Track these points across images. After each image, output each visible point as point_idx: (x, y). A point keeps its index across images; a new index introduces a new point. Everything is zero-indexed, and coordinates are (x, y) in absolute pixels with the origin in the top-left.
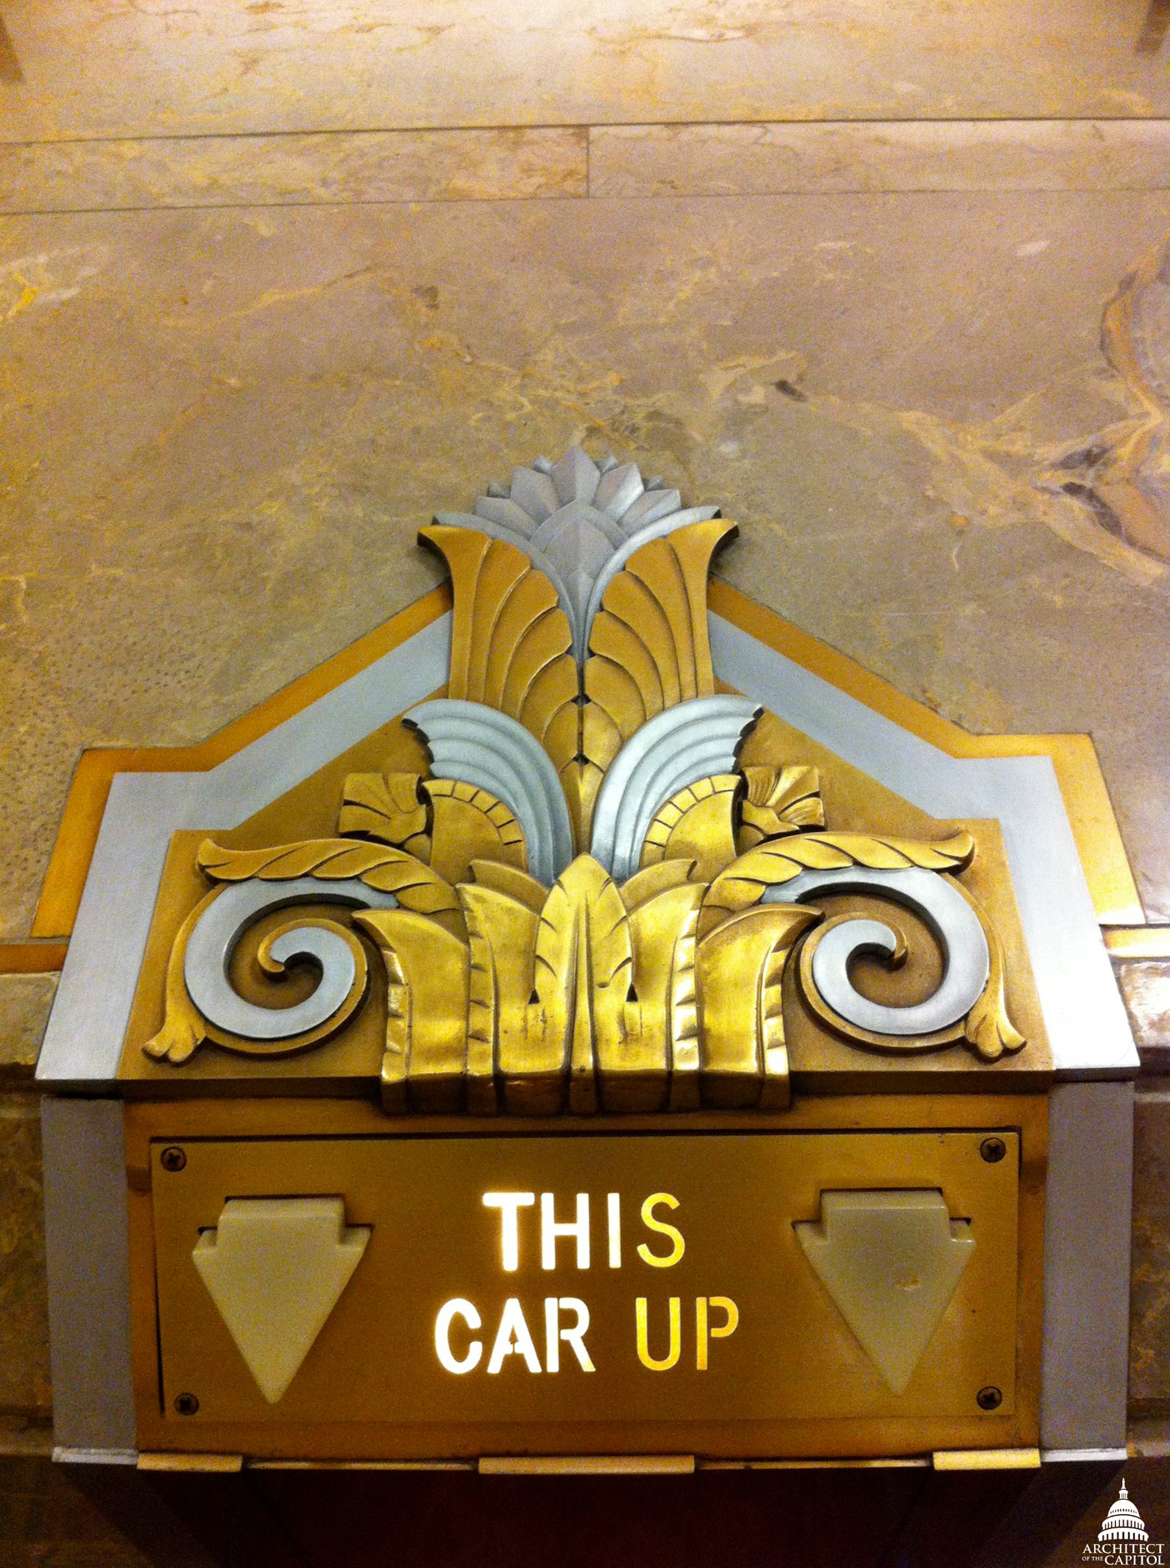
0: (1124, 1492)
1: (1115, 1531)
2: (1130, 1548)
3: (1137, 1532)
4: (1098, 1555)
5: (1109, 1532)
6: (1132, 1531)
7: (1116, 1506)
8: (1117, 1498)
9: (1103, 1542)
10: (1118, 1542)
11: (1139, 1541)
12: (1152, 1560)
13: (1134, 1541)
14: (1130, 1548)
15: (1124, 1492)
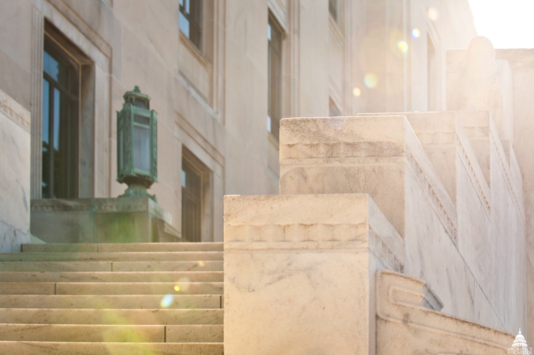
0: (520, 332)
8: (518, 334)
15: (520, 332)
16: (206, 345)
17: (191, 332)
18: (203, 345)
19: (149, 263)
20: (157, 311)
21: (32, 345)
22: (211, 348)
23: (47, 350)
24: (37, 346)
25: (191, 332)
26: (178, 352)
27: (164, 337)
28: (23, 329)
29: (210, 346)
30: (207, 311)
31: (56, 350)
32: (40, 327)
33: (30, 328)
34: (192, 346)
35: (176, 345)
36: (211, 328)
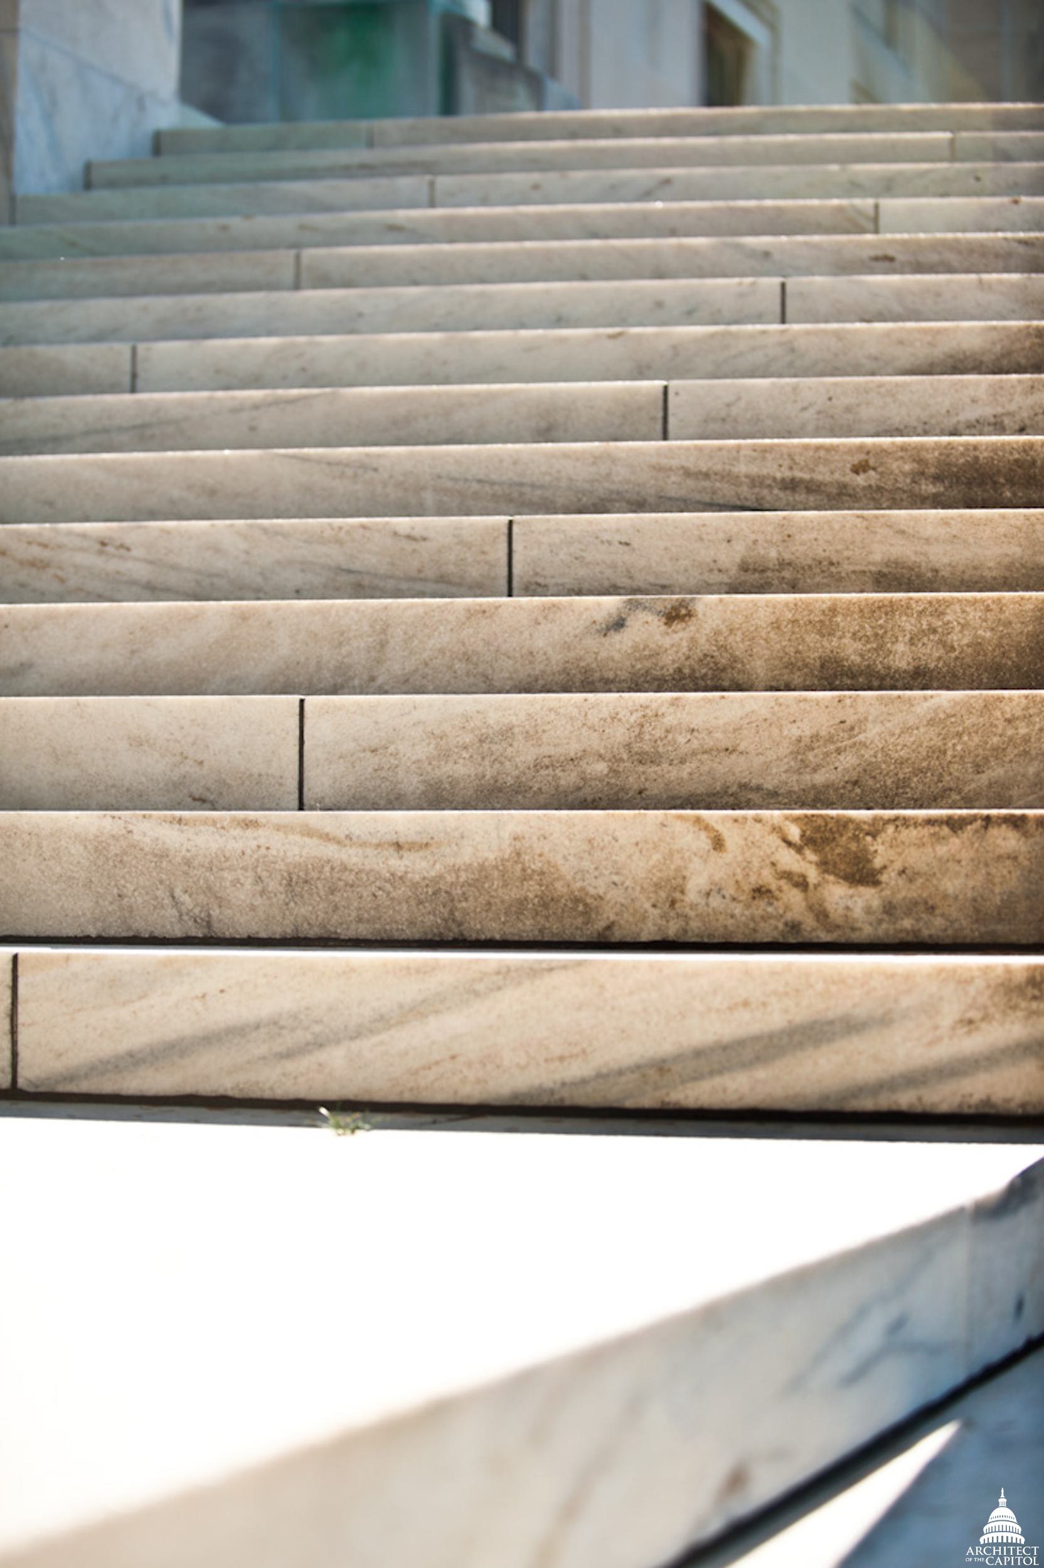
0: (1002, 1501)
1: (995, 1535)
2: (1008, 1551)
3: (1015, 1536)
4: (980, 1556)
5: (990, 1536)
6: (1010, 1535)
7: (996, 1513)
8: (997, 1506)
9: (983, 1546)
10: (997, 1545)
11: (1016, 1544)
12: (1028, 1561)
13: (1012, 1544)
14: (1008, 1551)
15: (1002, 1501)
16: (806, 447)
17: (739, 399)
18: (797, 446)
19: (535, 177)
20: (620, 334)
21: (305, 459)
22: (822, 453)
23: (349, 472)
24: (319, 461)
25: (739, 399)
26: (727, 467)
27: (660, 415)
28: (256, 407)
29: (818, 448)
30: (764, 332)
31: (376, 470)
32: (305, 398)
33: (277, 402)
34: (766, 450)
35: (720, 449)
36: (795, 388)
